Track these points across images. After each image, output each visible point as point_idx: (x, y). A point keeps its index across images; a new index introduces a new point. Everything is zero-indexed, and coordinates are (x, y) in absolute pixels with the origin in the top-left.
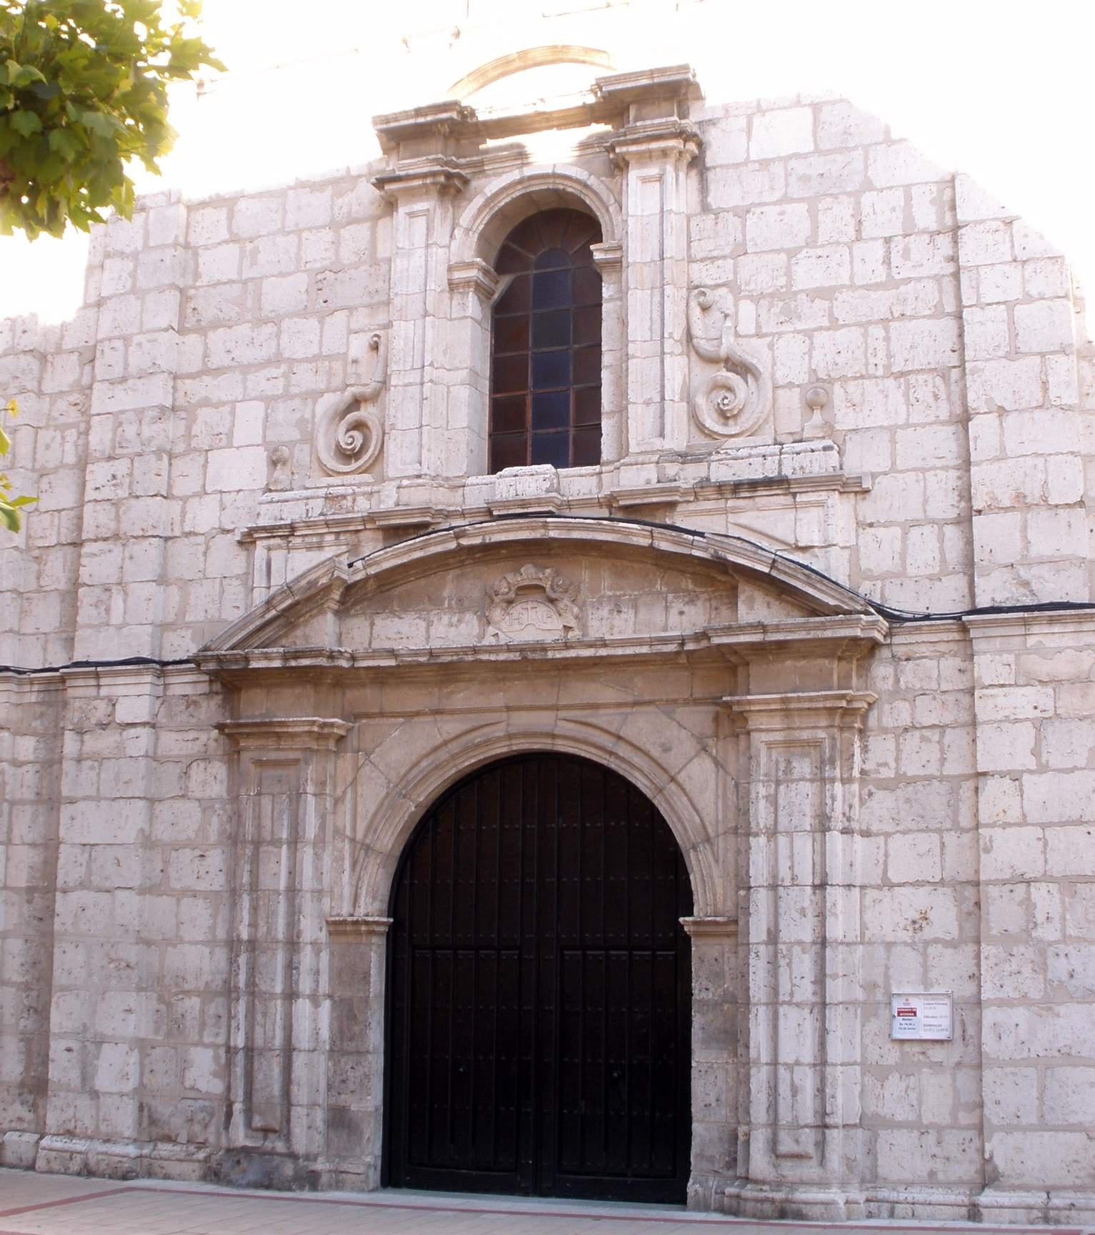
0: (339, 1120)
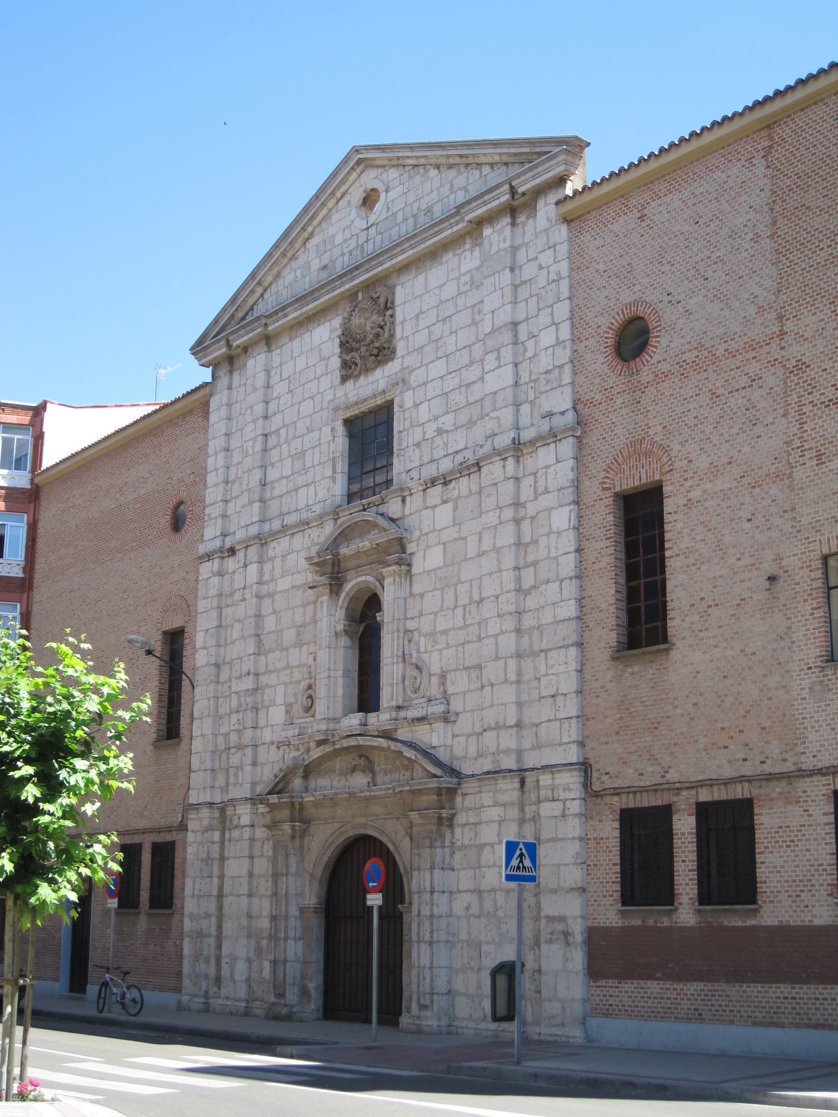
0: (304, 992)
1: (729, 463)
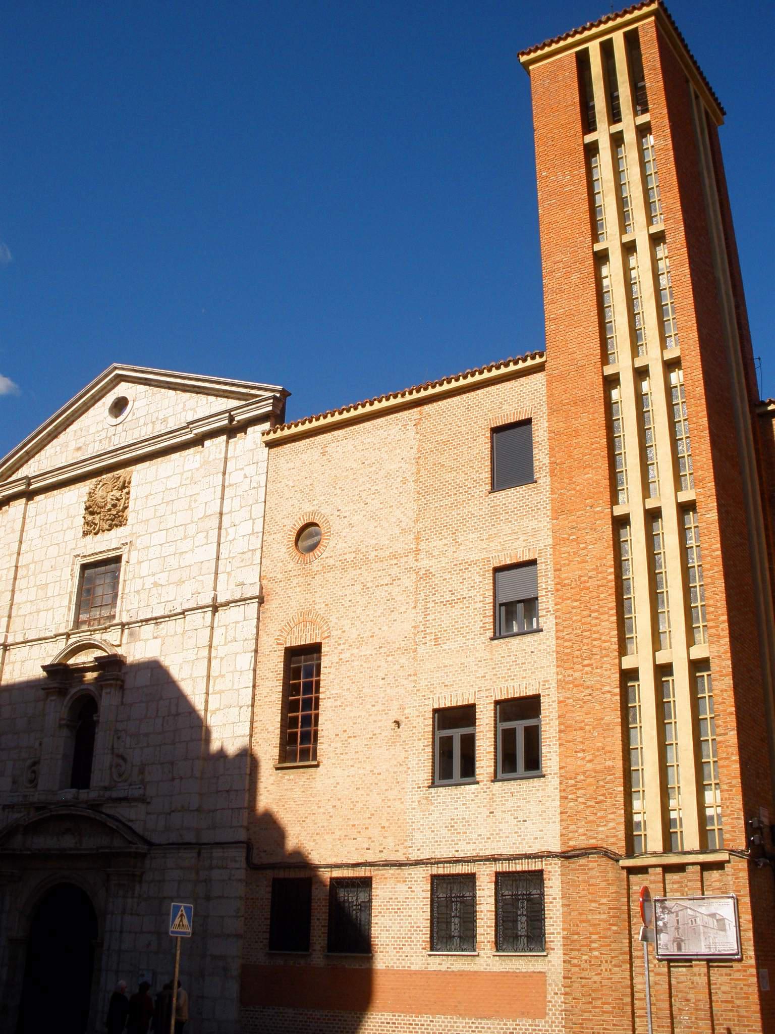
1: (372, 636)
